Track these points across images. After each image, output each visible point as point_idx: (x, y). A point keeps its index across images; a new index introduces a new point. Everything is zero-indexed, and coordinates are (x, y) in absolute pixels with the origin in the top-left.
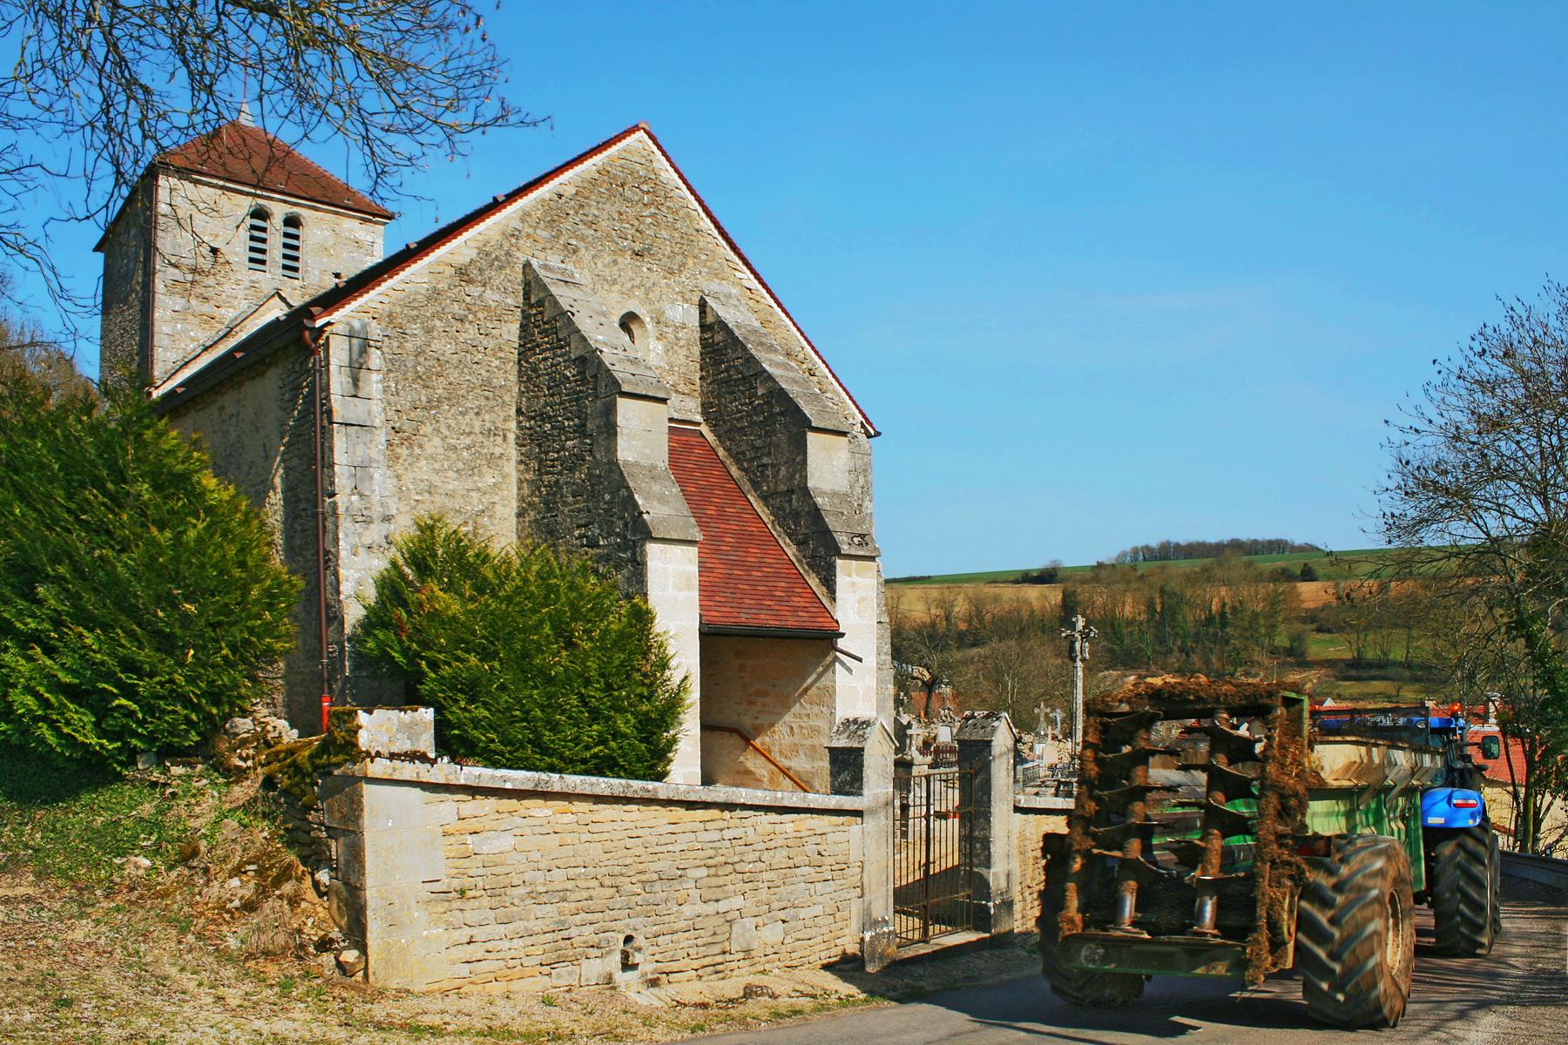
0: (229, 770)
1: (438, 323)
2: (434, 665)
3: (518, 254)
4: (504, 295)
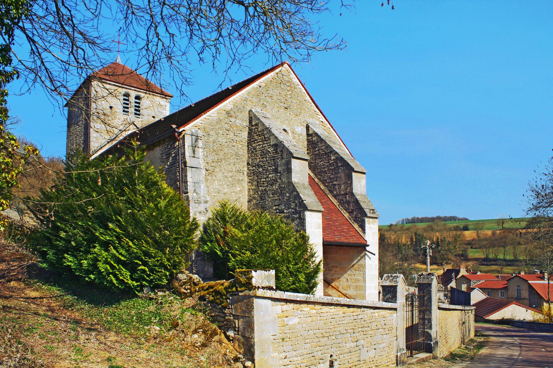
0: (181, 294)
1: (220, 131)
2: (234, 256)
3: (247, 107)
4: (243, 122)
